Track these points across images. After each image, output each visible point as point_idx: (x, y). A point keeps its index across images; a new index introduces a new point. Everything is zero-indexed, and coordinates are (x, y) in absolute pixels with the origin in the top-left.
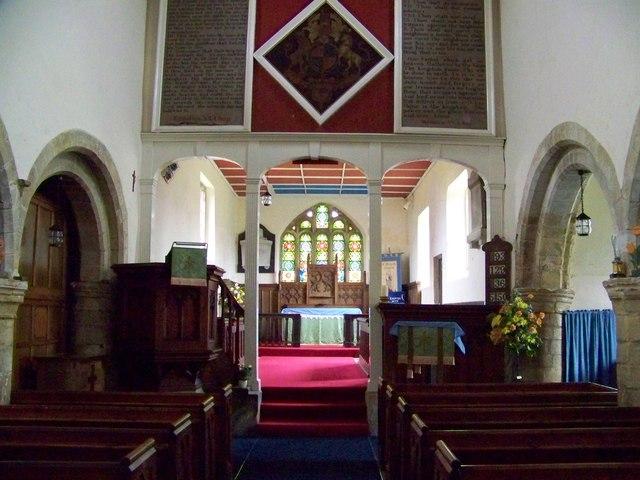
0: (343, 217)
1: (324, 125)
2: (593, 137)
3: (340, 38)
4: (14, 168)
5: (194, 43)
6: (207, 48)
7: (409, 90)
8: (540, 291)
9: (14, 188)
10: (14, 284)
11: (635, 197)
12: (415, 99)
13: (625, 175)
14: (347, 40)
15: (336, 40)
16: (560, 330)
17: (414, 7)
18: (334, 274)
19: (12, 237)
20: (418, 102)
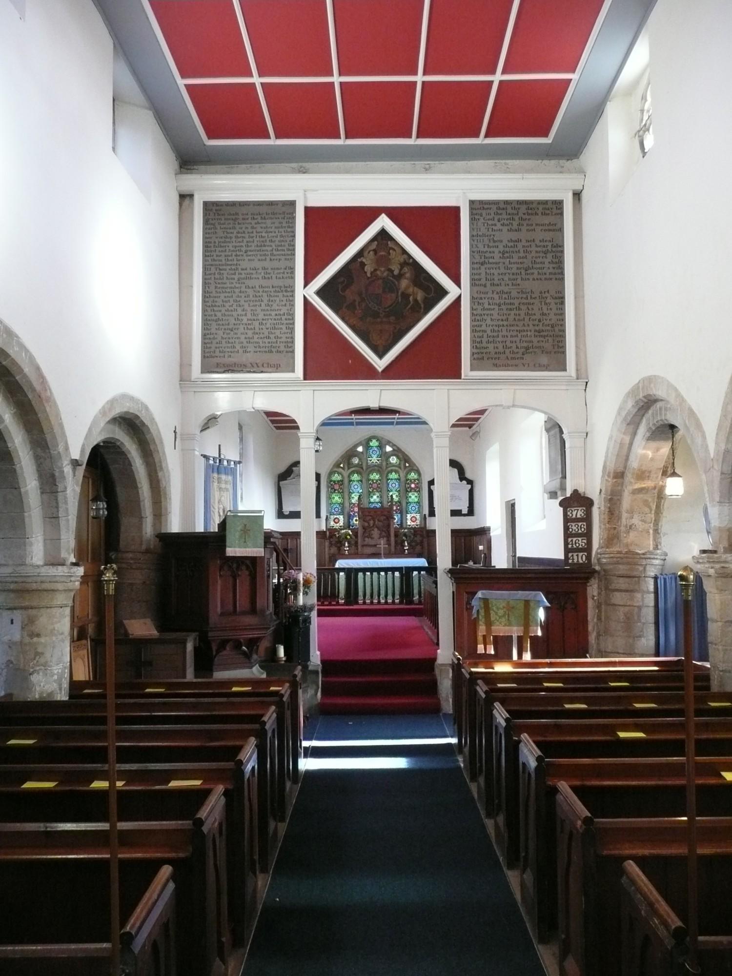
0: (397, 452)
1: (383, 371)
2: (682, 397)
3: (401, 270)
4: (67, 448)
5: (236, 277)
6: (250, 283)
7: (478, 329)
8: (626, 553)
9: (68, 469)
10: (72, 571)
11: (727, 469)
12: (485, 339)
13: (717, 443)
14: (408, 272)
15: (396, 272)
16: (652, 596)
17: (483, 230)
18: (390, 517)
19: (68, 521)
20: (488, 342)
